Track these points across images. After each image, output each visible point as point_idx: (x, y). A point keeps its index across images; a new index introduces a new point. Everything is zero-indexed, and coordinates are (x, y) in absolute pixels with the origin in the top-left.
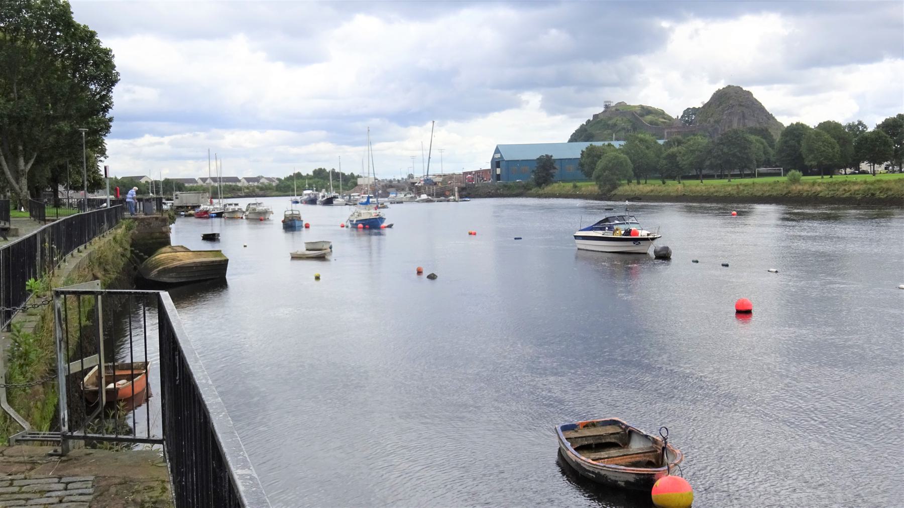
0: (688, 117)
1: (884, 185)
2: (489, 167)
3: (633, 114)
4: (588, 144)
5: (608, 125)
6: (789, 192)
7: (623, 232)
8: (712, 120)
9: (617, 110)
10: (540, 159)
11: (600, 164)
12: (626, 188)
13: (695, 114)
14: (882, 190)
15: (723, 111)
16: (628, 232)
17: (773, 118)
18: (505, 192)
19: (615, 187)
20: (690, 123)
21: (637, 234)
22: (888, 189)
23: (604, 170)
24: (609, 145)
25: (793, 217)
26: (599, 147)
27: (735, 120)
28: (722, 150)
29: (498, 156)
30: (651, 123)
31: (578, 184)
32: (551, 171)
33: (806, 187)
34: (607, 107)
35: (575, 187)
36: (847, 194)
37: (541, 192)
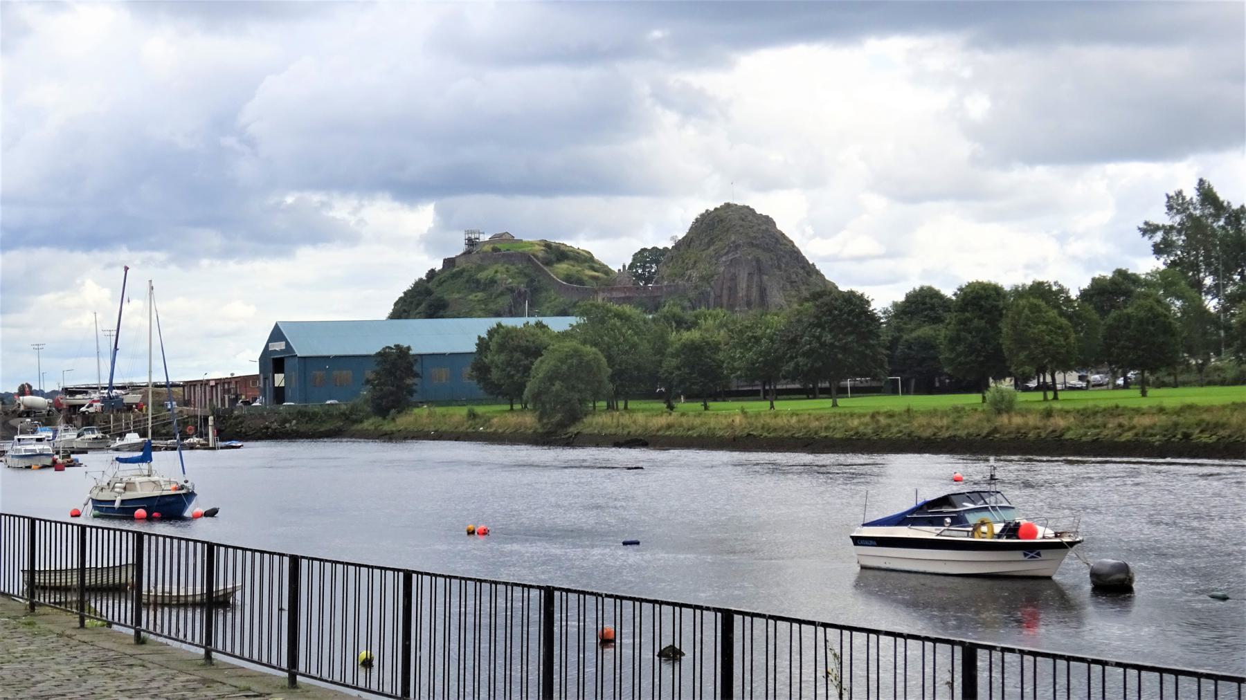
0: (644, 268)
1: (1206, 417)
2: (255, 370)
3: (528, 258)
4: (492, 322)
5: (478, 282)
6: (995, 430)
7: (998, 528)
8: (695, 274)
9: (495, 250)
10: (383, 355)
11: (541, 367)
12: (601, 419)
13: (657, 262)
14: (1205, 428)
15: (718, 255)
16: (1012, 529)
17: (818, 273)
18: (303, 428)
19: (574, 417)
20: (648, 280)
21: (1033, 534)
22: (1216, 425)
23: (551, 378)
24: (540, 325)
25: (27, 462)
26: (514, 329)
27: (743, 276)
28: (819, 338)
29: (279, 346)
30: (568, 278)
31: (480, 410)
32: (409, 381)
33: (1032, 420)
34: (471, 243)
35: (472, 415)
36: (1129, 435)
37: (388, 427)
